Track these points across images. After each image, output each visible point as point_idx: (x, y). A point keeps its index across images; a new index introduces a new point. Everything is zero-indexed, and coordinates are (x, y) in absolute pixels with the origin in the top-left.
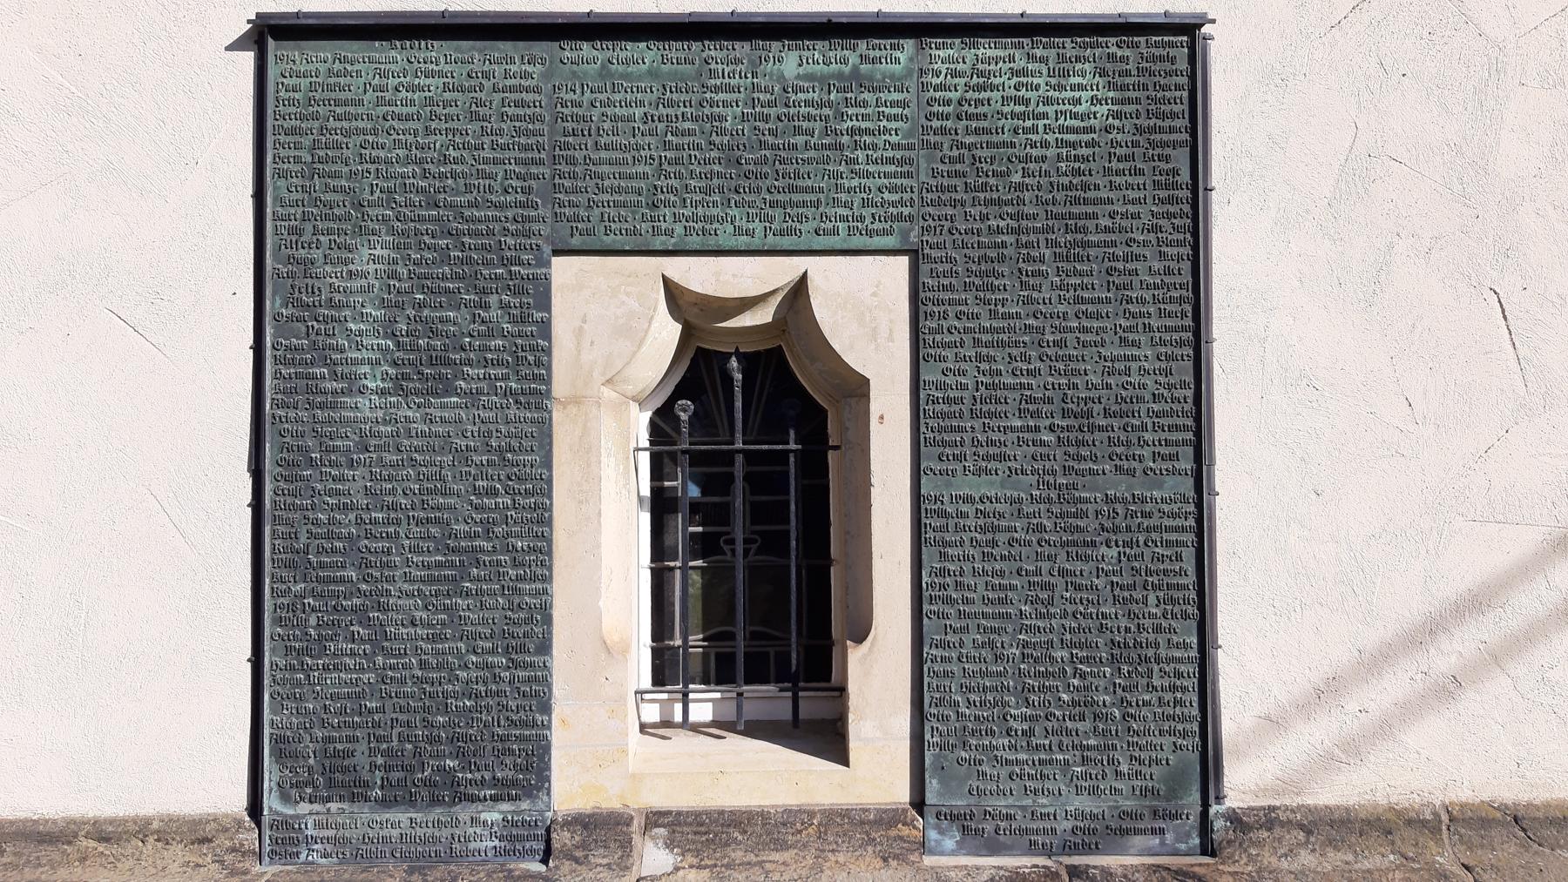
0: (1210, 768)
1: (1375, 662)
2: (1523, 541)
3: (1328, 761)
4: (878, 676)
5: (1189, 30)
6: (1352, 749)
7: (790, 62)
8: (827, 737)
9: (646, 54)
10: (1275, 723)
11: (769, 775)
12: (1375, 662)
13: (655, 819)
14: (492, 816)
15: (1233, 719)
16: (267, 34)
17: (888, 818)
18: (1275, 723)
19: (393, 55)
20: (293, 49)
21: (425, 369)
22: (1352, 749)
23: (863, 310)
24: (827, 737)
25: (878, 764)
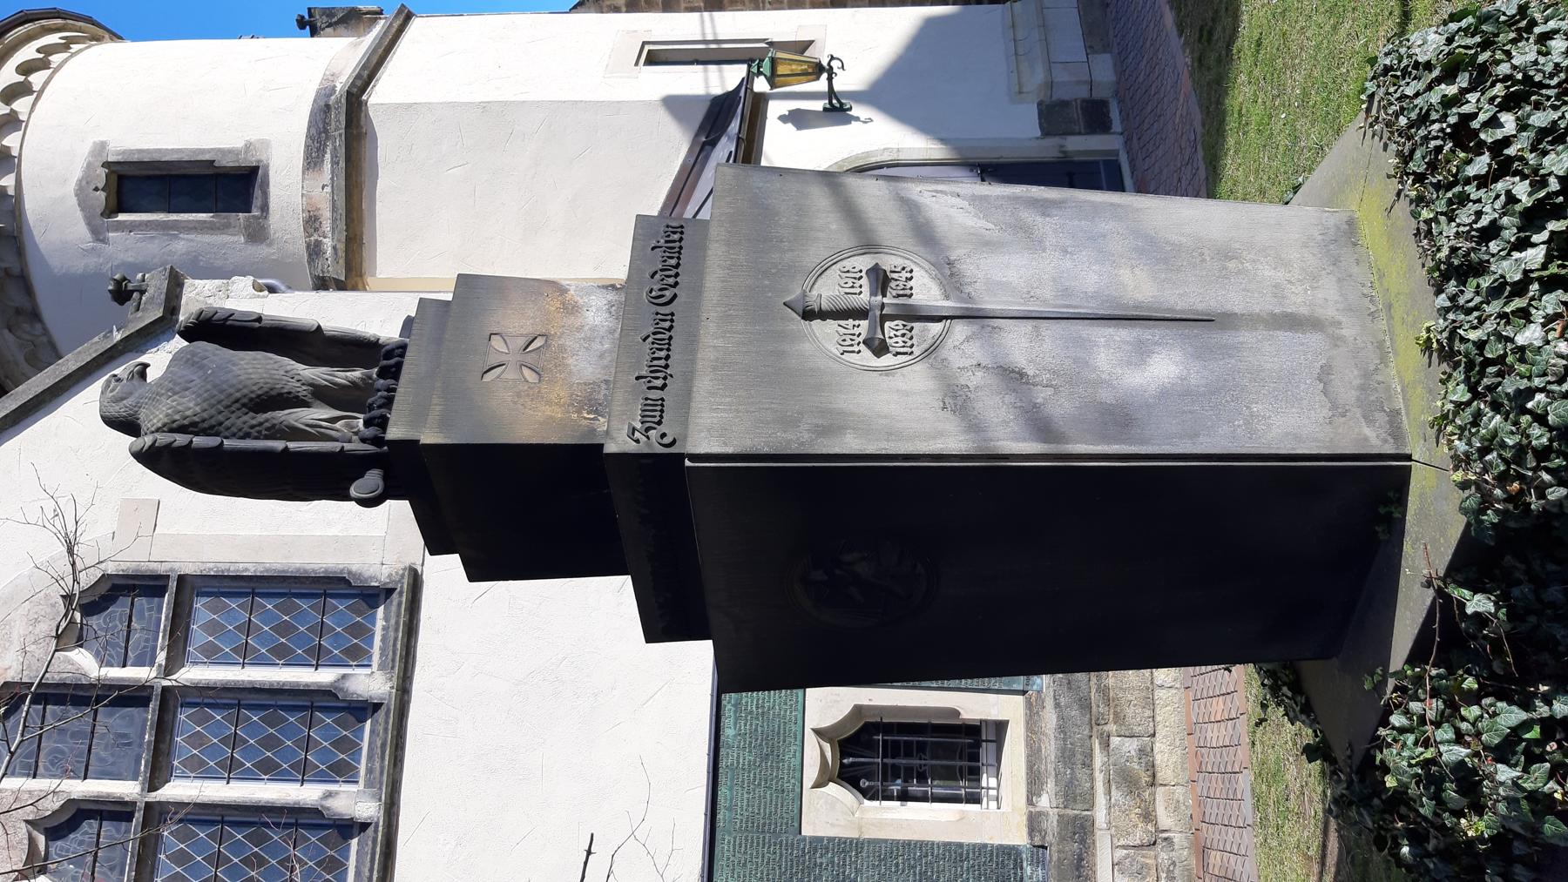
4: (972, 704)
7: (729, 732)
8: (1001, 727)
9: (723, 791)
13: (1030, 802)
14: (1028, 870)
24: (1001, 727)
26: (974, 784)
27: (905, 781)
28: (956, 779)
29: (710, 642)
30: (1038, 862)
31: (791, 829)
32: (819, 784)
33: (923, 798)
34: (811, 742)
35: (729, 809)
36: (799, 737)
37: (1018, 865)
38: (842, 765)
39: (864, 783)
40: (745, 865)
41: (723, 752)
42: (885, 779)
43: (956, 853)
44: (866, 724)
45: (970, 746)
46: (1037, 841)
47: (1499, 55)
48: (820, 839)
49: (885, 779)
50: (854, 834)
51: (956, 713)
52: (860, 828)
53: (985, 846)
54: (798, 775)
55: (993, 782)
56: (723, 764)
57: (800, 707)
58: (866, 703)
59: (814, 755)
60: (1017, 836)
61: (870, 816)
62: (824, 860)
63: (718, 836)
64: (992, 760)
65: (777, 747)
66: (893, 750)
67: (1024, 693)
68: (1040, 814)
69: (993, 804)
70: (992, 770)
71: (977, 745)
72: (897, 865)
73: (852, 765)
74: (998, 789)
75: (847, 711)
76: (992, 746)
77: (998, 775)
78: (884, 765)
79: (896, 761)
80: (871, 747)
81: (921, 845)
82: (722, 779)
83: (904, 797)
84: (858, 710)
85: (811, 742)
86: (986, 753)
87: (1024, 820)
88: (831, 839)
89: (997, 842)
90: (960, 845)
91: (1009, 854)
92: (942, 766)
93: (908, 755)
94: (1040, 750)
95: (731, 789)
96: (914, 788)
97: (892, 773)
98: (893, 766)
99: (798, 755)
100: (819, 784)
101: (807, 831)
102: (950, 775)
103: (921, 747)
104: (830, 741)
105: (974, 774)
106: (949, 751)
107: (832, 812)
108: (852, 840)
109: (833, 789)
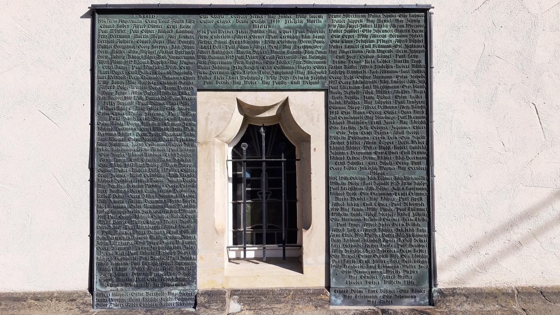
0: (432, 274)
1: (491, 237)
2: (544, 193)
3: (474, 272)
4: (313, 241)
5: (424, 11)
6: (483, 268)
7: (282, 22)
8: (295, 263)
9: (231, 19)
10: (455, 258)
11: (275, 277)
12: (491, 237)
13: (234, 292)
14: (176, 291)
15: (441, 257)
16: (95, 12)
17: (317, 292)
18: (455, 258)
19: (140, 20)
20: (105, 18)
21: (152, 132)
22: (483, 268)
23: (308, 111)
24: (295, 263)
25: (314, 273)
26: (249, 238)
27: (248, 181)
28: (252, 223)
29: (74, 276)
30: (184, 299)
31: (201, 82)
32: (241, 105)
33: (236, 196)
34: (276, 98)
35: (216, 26)
36: (281, 87)
37: (180, 282)
38: (260, 127)
39: (245, 147)
40: (169, 42)
41: (265, 17)
42: (249, 164)
43: (188, 227)
44: (294, 148)
45: (280, 235)
46: (200, 299)
47: (400, 247)
48: (195, 108)
49: (249, 164)
50: (200, 137)
51: (307, 226)
52: (206, 143)
53: (195, 253)
54: (248, 86)
55: (251, 254)
56: (255, 18)
57: (306, 86)
58: (313, 146)
59: (266, 100)
60: (204, 281)
61: (217, 152)
62: (177, 112)
63: (193, 17)
64: (269, 254)
65: (274, 66)
66: (273, 170)
67: (328, 287)
68: (224, 302)
69: (233, 255)
70: (261, 254)
71: (279, 241)
72: (176, 176)
73: (260, 135)
74: (245, 259)
75: (305, 128)
76: (280, 254)
77: (258, 259)
78: (260, 164)
79: (264, 173)
80: (274, 151)
81: (194, 197)
82: (241, 18)
83: (236, 180)
84: (306, 139)
85: (276, 98)
86: (274, 249)
87: (218, 286)
88: (195, 117)
89: (199, 263)
90: (195, 231)
91: (190, 275)
92: (261, 212)
93: (270, 183)
94: (279, 302)
95: (233, 26)
96: (244, 189)
97: (254, 168)
98: (261, 171)
99: (265, 86)
100: (241, 105)
101: (201, 96)
102: (256, 219)
103: (277, 194)
104: (279, 116)
105: (257, 240)
106: (275, 218)
107: (219, 119)
108: (195, 136)
109: (237, 120)
